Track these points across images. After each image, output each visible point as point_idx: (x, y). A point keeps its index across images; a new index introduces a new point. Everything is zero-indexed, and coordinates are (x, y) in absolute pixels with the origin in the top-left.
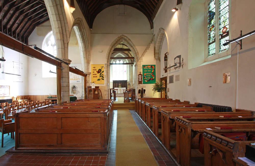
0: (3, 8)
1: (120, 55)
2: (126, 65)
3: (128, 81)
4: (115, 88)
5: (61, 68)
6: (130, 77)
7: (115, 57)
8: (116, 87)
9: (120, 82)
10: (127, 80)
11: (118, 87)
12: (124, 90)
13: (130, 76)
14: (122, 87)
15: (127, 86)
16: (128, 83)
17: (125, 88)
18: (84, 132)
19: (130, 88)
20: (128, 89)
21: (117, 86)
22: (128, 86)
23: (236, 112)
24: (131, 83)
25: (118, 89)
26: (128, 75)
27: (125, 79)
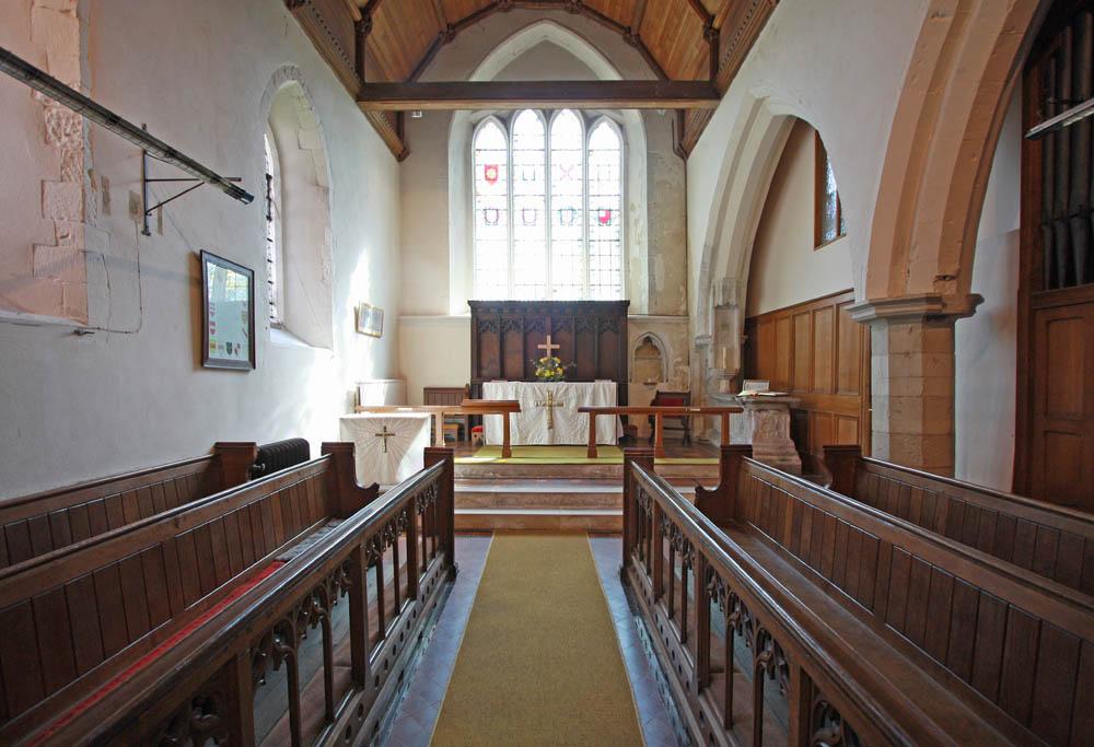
0: (814, 733)
1: (547, 46)
2: (372, 339)
3: (640, 305)
4: (495, 391)
5: (474, 448)
6: (659, 271)
7: (484, 73)
8: (503, 376)
9: (548, 323)
10: (626, 304)
11: (528, 376)
12: (594, 413)
13: (659, 259)
14: (571, 376)
15: (632, 364)
16: (635, 337)
17: (604, 392)
18: (181, 596)
19: (663, 387)
20: (640, 396)
21: (515, 363)
22: (640, 363)
23: (1013, 497)
24: (666, 339)
25: (514, 406)
26: (640, 252)
27: (610, 293)
